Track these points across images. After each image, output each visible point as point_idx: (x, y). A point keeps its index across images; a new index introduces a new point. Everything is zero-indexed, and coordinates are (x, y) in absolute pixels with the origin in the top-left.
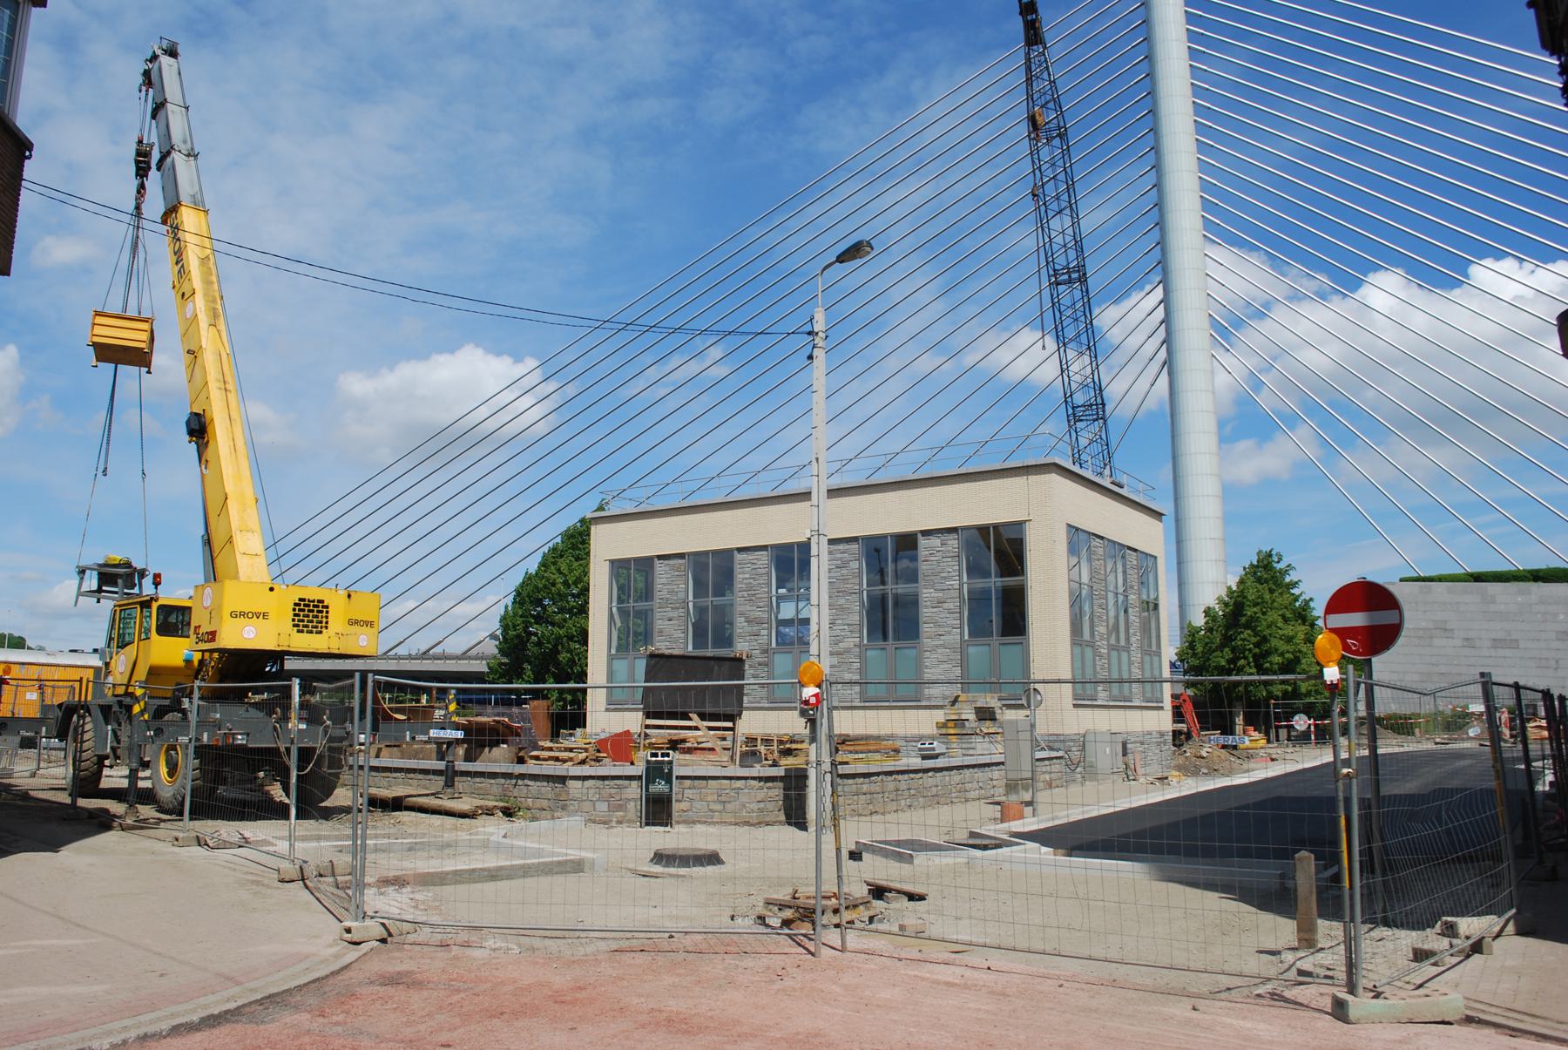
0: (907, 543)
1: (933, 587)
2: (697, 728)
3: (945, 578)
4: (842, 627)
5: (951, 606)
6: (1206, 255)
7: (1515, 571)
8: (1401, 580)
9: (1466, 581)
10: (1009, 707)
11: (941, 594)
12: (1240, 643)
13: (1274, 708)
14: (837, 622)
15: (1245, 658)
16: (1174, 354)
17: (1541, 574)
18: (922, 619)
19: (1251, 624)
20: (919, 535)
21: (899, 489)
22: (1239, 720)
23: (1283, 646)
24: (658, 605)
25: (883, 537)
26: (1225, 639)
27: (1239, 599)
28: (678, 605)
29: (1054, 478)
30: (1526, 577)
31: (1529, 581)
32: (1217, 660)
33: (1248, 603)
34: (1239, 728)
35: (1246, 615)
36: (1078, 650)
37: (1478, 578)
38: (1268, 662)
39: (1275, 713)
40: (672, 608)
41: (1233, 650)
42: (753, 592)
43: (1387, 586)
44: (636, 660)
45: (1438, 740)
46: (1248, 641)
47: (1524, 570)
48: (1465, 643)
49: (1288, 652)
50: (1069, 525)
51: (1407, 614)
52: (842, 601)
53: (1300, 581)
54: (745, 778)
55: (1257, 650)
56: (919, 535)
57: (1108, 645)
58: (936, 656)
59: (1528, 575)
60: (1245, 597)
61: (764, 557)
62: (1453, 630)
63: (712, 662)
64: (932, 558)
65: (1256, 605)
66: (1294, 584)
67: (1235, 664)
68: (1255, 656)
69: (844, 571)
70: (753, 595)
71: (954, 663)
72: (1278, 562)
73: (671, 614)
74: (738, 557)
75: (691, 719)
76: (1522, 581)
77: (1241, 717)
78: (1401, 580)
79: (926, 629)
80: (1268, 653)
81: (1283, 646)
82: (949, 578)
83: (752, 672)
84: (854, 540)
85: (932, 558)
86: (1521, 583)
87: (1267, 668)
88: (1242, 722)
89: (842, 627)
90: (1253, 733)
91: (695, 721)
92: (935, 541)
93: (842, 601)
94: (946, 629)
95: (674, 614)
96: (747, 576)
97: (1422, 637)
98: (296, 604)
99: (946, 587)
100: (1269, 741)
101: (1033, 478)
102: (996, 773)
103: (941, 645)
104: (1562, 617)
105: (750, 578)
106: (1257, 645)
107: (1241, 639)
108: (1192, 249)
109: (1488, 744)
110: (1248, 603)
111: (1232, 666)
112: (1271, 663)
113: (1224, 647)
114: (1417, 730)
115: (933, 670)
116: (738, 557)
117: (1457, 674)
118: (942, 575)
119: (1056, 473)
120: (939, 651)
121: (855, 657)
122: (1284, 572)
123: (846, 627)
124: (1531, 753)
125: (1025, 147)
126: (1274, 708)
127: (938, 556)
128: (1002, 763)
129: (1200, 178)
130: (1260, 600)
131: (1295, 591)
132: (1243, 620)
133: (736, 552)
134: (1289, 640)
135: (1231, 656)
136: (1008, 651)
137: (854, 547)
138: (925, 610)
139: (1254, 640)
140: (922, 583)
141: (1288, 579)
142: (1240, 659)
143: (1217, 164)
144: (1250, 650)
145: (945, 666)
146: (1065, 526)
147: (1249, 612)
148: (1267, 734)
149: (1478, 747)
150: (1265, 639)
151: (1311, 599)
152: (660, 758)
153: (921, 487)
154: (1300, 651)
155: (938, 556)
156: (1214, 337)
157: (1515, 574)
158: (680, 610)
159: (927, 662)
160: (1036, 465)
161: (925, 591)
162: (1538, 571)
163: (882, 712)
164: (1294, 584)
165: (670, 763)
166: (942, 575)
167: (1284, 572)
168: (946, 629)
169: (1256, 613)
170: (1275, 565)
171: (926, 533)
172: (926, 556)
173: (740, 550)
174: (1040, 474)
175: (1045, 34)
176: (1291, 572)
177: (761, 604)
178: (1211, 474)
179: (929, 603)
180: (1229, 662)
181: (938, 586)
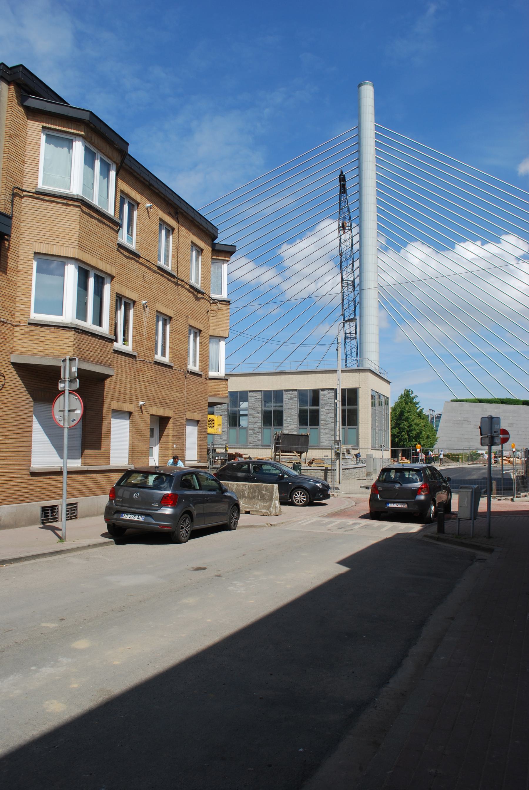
0: (316, 393)
1: (324, 408)
2: (295, 456)
3: (329, 405)
4: (290, 421)
5: (331, 415)
6: (378, 257)
7: (494, 399)
8: (451, 401)
9: (476, 402)
10: (353, 449)
11: (327, 411)
12: (403, 426)
13: (412, 451)
14: (288, 419)
15: (404, 432)
16: (363, 300)
17: (504, 401)
18: (320, 419)
19: (407, 419)
20: (320, 390)
21: (313, 374)
22: (400, 455)
23: (417, 428)
24: (216, 410)
25: (306, 390)
26: (396, 424)
27: (403, 410)
28: (224, 410)
29: (369, 374)
30: (499, 402)
31: (500, 403)
32: (393, 432)
33: (405, 411)
34: (400, 458)
35: (405, 416)
36: (372, 430)
37: (481, 401)
38: (412, 433)
39: (412, 452)
40: (222, 411)
41: (399, 429)
42: (255, 407)
43: (508, 431)
44: (230, 430)
45: (470, 464)
46: (405, 425)
47: (498, 399)
48: (475, 427)
49: (417, 430)
50: (372, 390)
51: (510, 435)
52: (290, 412)
53: (419, 402)
54: (318, 470)
55: (408, 429)
56: (320, 390)
57: (378, 429)
58: (325, 432)
59: (499, 401)
60: (405, 409)
61: (260, 395)
62: (470, 421)
63: (300, 436)
64: (324, 398)
65: (409, 412)
66: (417, 403)
67: (400, 434)
68: (407, 431)
69: (291, 401)
70: (255, 408)
71: (331, 434)
72: (411, 394)
73: (221, 413)
74: (249, 394)
75: (294, 453)
76: (497, 403)
77: (401, 454)
78: (451, 401)
79: (321, 422)
80: (411, 431)
81: (417, 428)
82: (331, 406)
83: (255, 435)
84: (296, 390)
85: (324, 398)
86: (497, 404)
87: (411, 436)
88: (401, 456)
89: (290, 421)
90: (405, 460)
91: (295, 454)
92: (326, 393)
93: (290, 412)
94: (329, 423)
95: (223, 413)
96: (253, 401)
97: (459, 424)
98: (213, 419)
99: (329, 409)
100: (411, 462)
101: (362, 374)
102: (363, 470)
103: (327, 428)
104: (511, 418)
105: (254, 402)
106: (408, 427)
107: (403, 425)
108: (373, 255)
109: (487, 465)
110: (405, 411)
111: (399, 435)
112: (413, 434)
113: (396, 427)
114: (460, 460)
115: (324, 437)
116: (249, 394)
117: (471, 439)
118: (328, 404)
119: (370, 373)
120: (326, 430)
121: (295, 431)
122: (413, 398)
123: (292, 421)
124: (504, 469)
125: (336, 233)
126: (412, 451)
127: (327, 398)
128: (365, 467)
129: (377, 223)
130: (410, 410)
131: (418, 406)
132: (404, 418)
133: (249, 392)
134: (418, 425)
135: (399, 431)
136: (351, 431)
137: (296, 393)
138: (321, 416)
139: (408, 425)
140: (320, 406)
141: (414, 401)
142: (403, 432)
143: (385, 218)
144: (406, 429)
145: (328, 435)
146: (370, 390)
147: (406, 415)
148: (410, 460)
149: (483, 466)
150: (411, 425)
151: (423, 409)
152: (298, 464)
153: (321, 374)
154: (422, 430)
155: (327, 398)
156: (379, 293)
157: (495, 400)
158: (226, 412)
159: (322, 434)
160: (363, 369)
161: (321, 409)
162: (503, 399)
163: (316, 450)
164: (417, 403)
165: (301, 465)
166: (328, 404)
167: (413, 398)
168: (329, 423)
169: (409, 415)
170: (410, 395)
171: (322, 390)
172: (322, 397)
173: (250, 391)
174: (364, 372)
175: (347, 190)
176: (416, 398)
177: (259, 411)
178: (375, 352)
179: (323, 414)
180: (398, 433)
181: (326, 408)
